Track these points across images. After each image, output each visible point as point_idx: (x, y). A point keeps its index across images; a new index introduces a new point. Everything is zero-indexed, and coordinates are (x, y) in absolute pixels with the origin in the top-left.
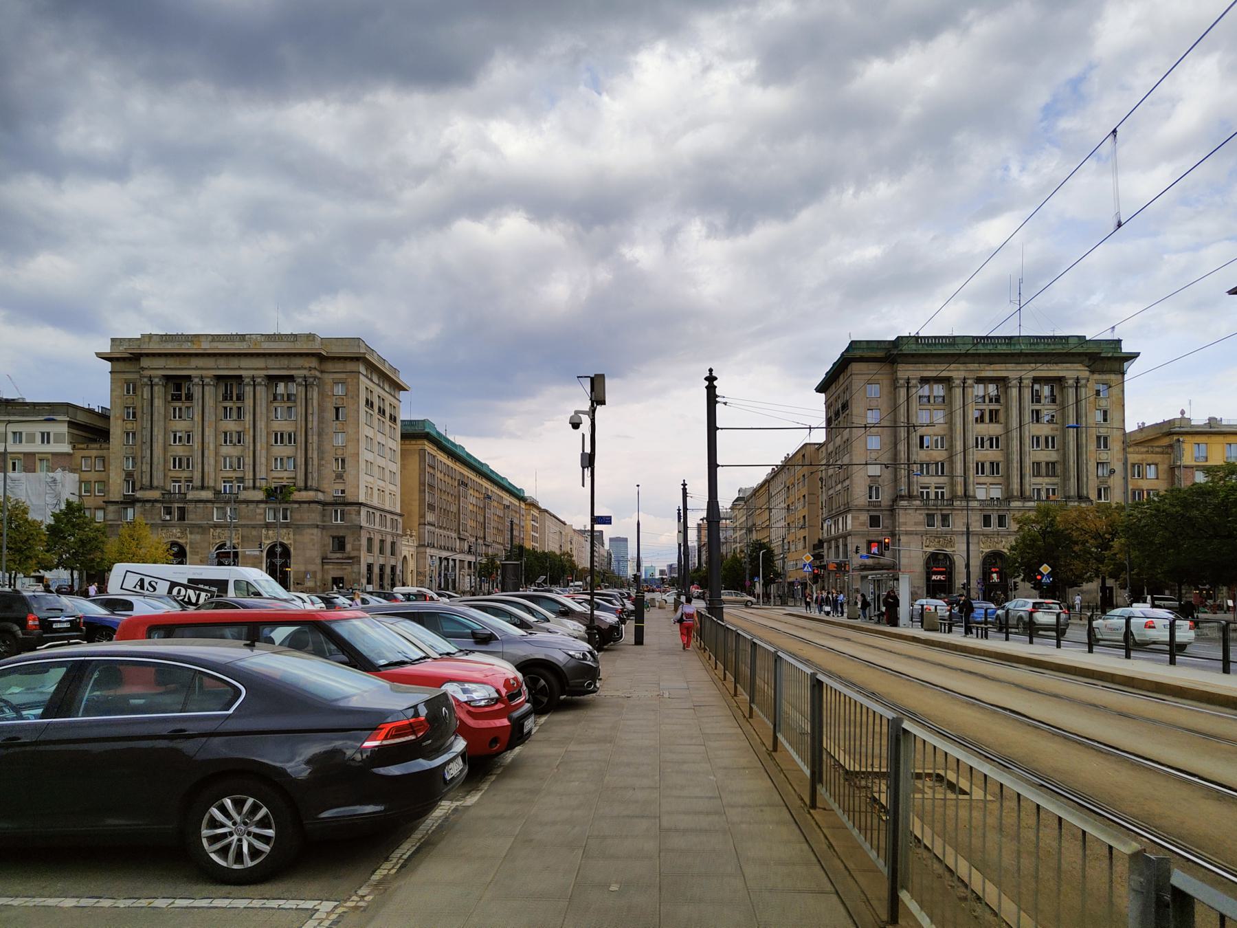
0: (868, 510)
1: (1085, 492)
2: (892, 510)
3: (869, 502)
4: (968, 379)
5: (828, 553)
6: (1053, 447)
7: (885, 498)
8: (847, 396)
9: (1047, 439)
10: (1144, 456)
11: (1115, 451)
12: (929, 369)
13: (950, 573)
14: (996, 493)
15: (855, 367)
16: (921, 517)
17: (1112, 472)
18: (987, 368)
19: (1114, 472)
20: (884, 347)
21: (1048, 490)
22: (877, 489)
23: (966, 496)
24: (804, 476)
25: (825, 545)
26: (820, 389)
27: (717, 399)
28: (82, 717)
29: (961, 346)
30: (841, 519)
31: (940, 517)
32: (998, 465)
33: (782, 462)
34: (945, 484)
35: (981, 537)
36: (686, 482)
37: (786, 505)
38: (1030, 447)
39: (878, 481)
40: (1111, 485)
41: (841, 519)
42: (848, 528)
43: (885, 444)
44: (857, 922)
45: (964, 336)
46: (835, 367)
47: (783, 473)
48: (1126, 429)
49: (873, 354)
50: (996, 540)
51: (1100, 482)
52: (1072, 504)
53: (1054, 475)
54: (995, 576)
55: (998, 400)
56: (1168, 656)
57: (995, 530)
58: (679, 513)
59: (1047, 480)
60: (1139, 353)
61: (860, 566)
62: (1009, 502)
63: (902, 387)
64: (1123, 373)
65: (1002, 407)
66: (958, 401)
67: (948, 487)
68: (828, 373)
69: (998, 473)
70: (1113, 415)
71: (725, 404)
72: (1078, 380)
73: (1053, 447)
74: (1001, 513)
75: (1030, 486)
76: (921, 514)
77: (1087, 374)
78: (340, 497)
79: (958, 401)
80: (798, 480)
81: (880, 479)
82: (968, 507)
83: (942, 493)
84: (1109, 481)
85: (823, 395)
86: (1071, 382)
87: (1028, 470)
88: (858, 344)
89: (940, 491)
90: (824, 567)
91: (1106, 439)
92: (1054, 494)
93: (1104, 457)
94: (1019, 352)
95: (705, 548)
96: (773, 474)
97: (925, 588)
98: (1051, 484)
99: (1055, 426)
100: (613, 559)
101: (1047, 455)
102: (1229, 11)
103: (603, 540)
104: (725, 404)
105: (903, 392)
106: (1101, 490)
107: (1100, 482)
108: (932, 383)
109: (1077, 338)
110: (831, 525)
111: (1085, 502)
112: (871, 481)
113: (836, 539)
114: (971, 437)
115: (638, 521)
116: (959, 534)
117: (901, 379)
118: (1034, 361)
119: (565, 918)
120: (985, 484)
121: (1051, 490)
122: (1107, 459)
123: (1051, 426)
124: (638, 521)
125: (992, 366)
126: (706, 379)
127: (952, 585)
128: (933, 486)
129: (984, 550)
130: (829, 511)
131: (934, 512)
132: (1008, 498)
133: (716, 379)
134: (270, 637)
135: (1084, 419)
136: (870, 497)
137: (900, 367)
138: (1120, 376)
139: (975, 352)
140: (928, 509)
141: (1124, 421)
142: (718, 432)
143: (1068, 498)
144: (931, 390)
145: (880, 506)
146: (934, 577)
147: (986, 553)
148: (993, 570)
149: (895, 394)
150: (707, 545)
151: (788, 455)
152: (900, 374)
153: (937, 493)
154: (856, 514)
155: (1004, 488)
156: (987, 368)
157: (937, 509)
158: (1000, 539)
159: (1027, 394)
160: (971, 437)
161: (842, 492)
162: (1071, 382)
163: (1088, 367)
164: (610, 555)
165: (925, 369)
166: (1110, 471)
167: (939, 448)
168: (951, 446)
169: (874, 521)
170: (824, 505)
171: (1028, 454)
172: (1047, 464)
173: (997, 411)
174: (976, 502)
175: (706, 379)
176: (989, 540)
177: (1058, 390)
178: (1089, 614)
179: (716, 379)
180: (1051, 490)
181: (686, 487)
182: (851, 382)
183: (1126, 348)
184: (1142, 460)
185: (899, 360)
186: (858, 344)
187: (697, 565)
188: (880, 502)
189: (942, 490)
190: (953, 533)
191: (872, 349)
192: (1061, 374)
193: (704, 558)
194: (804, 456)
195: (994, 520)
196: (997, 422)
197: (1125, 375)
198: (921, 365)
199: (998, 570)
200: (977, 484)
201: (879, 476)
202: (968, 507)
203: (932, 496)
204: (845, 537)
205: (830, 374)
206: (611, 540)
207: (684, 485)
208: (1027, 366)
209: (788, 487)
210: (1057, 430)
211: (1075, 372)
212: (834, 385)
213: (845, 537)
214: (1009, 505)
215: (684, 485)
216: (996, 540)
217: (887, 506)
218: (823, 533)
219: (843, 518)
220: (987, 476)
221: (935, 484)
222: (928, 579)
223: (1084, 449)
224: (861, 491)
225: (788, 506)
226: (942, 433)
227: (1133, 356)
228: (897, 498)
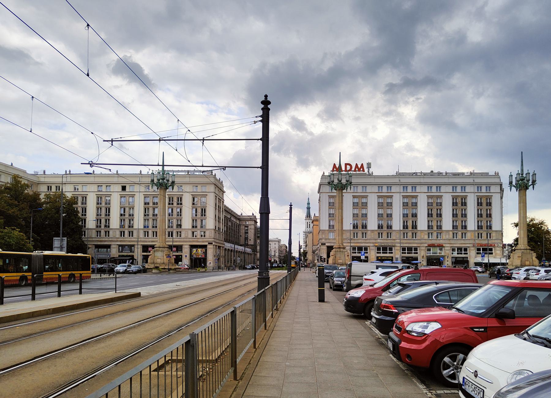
27: (261, 119)
36: (269, 99)
56: (516, 316)
82: (62, 182)
119: (356, 396)
126: (262, 103)
133: (292, 205)
134: (527, 271)
142: (260, 165)
175: (262, 103)
179: (292, 205)
181: (292, 206)
202: (62, 182)
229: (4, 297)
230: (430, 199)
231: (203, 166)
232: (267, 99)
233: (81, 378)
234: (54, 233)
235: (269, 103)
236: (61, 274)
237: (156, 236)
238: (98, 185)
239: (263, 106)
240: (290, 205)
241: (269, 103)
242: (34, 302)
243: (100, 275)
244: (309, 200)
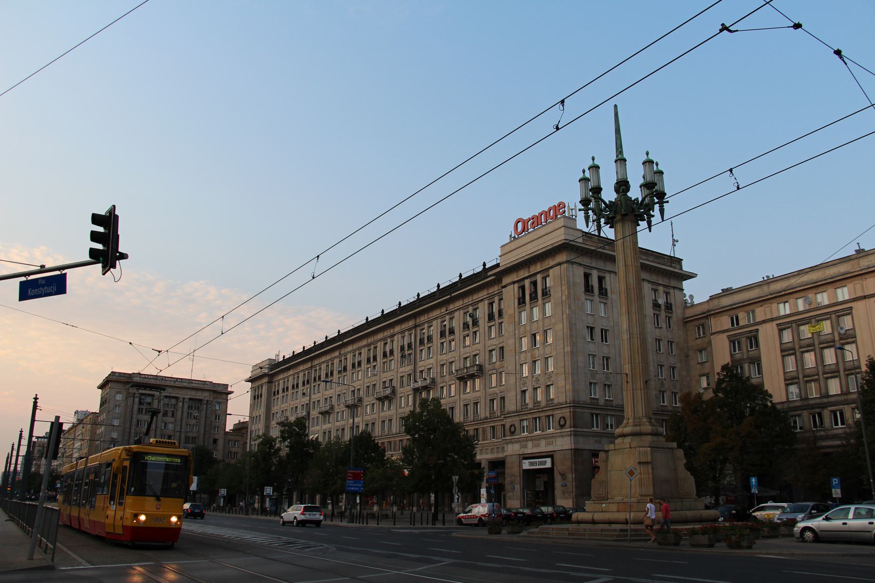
27: (38, 408)
36: (38, 397)
44: (52, 438)
58: (8, 456)
71: (41, 410)
78: (758, 377)
85: (100, 390)
102: (743, 17)
104: (41, 410)
115: (231, 415)
124: (231, 415)
133: (38, 399)
136: (655, 325)
142: (36, 422)
159: (137, 400)
178: (725, 421)
179: (38, 399)
181: (38, 400)
195: (170, 414)
207: (36, 399)
215: (36, 399)
227: (232, 392)
229: (228, 413)
230: (813, 383)
231: (593, 520)
233: (641, 384)
236: (160, 414)
237: (219, 420)
239: (34, 400)
244: (559, 122)
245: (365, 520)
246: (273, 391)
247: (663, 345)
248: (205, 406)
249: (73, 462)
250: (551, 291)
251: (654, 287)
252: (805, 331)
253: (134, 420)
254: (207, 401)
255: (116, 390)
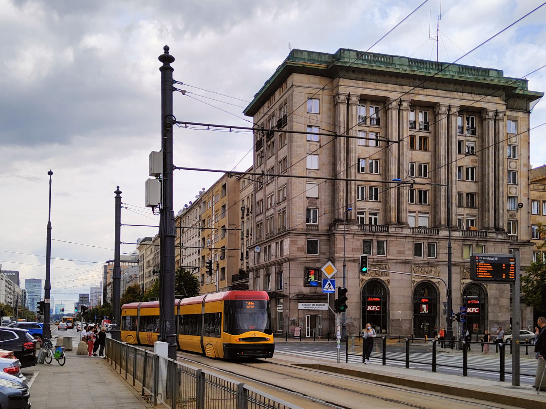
0: (307, 235)
1: (501, 224)
2: (330, 235)
3: (307, 225)
4: (404, 101)
5: (254, 282)
6: (472, 179)
7: (322, 222)
8: (286, 110)
9: (467, 169)
10: (541, 193)
11: (522, 186)
12: (368, 86)
13: (384, 303)
14: (423, 222)
15: (297, 78)
16: (359, 242)
17: (520, 206)
18: (421, 92)
19: (522, 206)
20: (324, 60)
21: (468, 220)
22: (315, 212)
23: (400, 223)
24: (224, 207)
25: (251, 275)
26: (251, 111)
28: (32, 335)
29: (398, 67)
30: (274, 245)
31: (376, 244)
32: (425, 193)
33: (196, 196)
34: (379, 210)
35: (413, 266)
36: (120, 190)
37: (200, 239)
38: (456, 176)
39: (316, 204)
40: (519, 220)
41: (274, 245)
42: (285, 254)
43: (324, 164)
45: (401, 57)
46: (268, 85)
47: (198, 208)
48: (531, 163)
49: (315, 65)
50: (426, 269)
51: (510, 215)
52: (491, 235)
53: (473, 207)
54: (424, 306)
55: (426, 128)
57: (426, 259)
59: (468, 211)
60: (543, 93)
61: (297, 295)
62: (438, 230)
63: (342, 103)
64: (529, 112)
65: (431, 135)
66: (394, 123)
67: (381, 214)
68: (257, 94)
69: (425, 202)
70: (522, 151)
71: (126, 208)
72: (496, 113)
73: (472, 179)
74: (431, 241)
75: (456, 215)
76: (358, 240)
77: (502, 108)
79: (394, 123)
80: (216, 211)
81: (318, 202)
83: (376, 219)
84: (517, 214)
86: (491, 114)
87: (454, 200)
88: (299, 53)
89: (373, 217)
90: (418, 270)
91: (515, 173)
92: (472, 225)
93: (513, 191)
94: (450, 77)
95: (110, 286)
96: (185, 211)
97: (361, 319)
98: (470, 215)
99: (475, 158)
100: (27, 297)
101: (470, 187)
103: (18, 280)
105: (343, 108)
106: (510, 223)
107: (510, 215)
108: (368, 103)
109: (496, 72)
110: (259, 254)
111: (501, 234)
112: (309, 203)
113: (267, 267)
114: (405, 161)
116: (394, 263)
117: (343, 94)
118: (461, 90)
120: (414, 212)
121: (470, 221)
122: (516, 194)
123: (472, 157)
125: (425, 90)
126: (161, 58)
127: (386, 316)
128: (367, 211)
129: (416, 280)
130: (257, 239)
131: (371, 238)
132: (436, 227)
133: (121, 192)
135: (501, 152)
137: (342, 82)
138: (527, 114)
139: (412, 73)
140: (365, 235)
141: (529, 157)
143: (487, 230)
144: (367, 111)
145: (318, 230)
146: (369, 308)
147: (418, 282)
148: (423, 300)
149: (335, 111)
150: (112, 284)
151: (204, 189)
152: (341, 90)
153: (370, 219)
154: (294, 238)
155: (430, 217)
156: (421, 92)
157: (374, 235)
158: (430, 268)
160: (405, 161)
161: (276, 216)
162: (491, 114)
163: (505, 101)
164: (25, 293)
165: (365, 86)
166: (519, 205)
167: (374, 172)
168: (386, 171)
169: (312, 247)
170: (250, 233)
171: (454, 183)
172: (468, 195)
173: (426, 138)
174: (409, 230)
175: (161, 58)
176: (420, 269)
177: (477, 122)
179: (121, 192)
180: (470, 221)
181: (121, 195)
182: (291, 95)
183: (532, 87)
184: (540, 198)
185: (341, 74)
186: (299, 53)
187: (102, 304)
188: (317, 226)
189: (376, 217)
190: (388, 261)
191: (313, 60)
192: (483, 105)
193: (109, 295)
194: (224, 186)
196: (426, 150)
197: (531, 114)
198: (360, 82)
199: (427, 300)
200: (410, 212)
201: (318, 198)
203: (367, 222)
204: (279, 264)
205: (259, 96)
206: (27, 281)
207: (118, 192)
208: (455, 94)
209: (204, 221)
210: (476, 162)
211: (494, 105)
212: (266, 105)
213: (279, 264)
214: (438, 234)
215: (118, 192)
216: (426, 269)
217: (325, 230)
218: (242, 264)
219: (277, 243)
220: (416, 204)
221: (369, 209)
222: (364, 310)
223: (501, 182)
224: (300, 214)
225: (204, 239)
226: (377, 156)
227: (537, 96)
228: (335, 222)
232: (169, 53)
234: (421, 327)
235: (172, 59)
238: (200, 241)
239: (161, 64)
240: (115, 192)
241: (172, 59)
242: (407, 370)
243: (285, 339)
245: (262, 401)
246: (241, 206)
247: (417, 271)
248: (491, 123)
249: (464, 111)
250: (102, 267)
251: (429, 168)
252: (467, 218)
253: (431, 128)
254: (496, 113)
255: (307, 90)
